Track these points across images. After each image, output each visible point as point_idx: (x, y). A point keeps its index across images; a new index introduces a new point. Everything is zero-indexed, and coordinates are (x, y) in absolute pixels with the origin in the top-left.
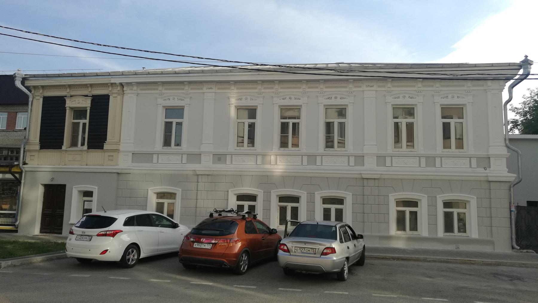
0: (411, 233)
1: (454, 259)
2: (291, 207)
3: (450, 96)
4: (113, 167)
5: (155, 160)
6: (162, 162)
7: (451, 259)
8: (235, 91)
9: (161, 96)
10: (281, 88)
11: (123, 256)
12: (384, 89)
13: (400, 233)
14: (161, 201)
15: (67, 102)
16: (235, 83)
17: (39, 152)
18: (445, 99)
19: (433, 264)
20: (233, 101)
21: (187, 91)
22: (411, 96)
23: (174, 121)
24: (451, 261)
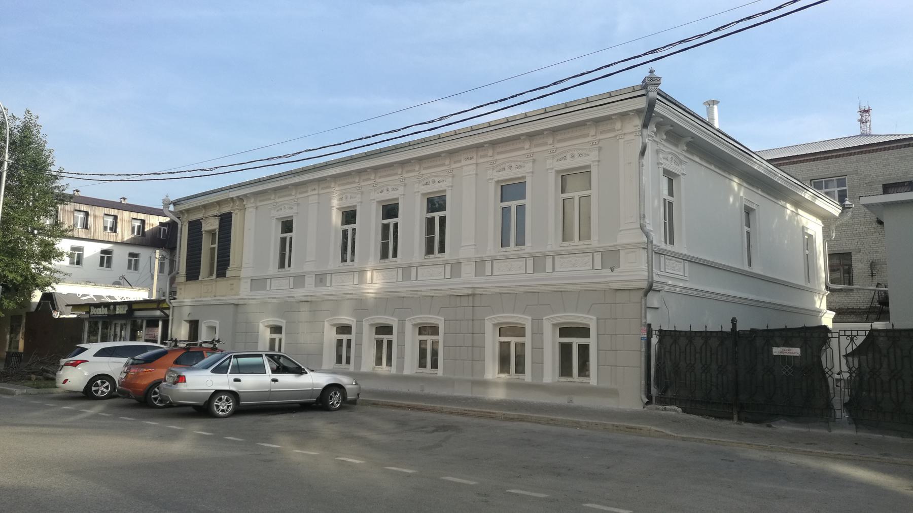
0: (517, 377)
1: (472, 411)
2: (579, 345)
3: (568, 155)
4: (224, 298)
5: (549, 268)
6: (561, 270)
7: (469, 411)
8: (337, 189)
9: (552, 154)
10: (558, 141)
11: (86, 387)
12: (587, 140)
13: (504, 376)
14: (504, 339)
15: (203, 225)
16: (554, 131)
17: (216, 281)
18: (563, 162)
19: (409, 412)
20: (335, 202)
21: (595, 137)
22: (519, 164)
23: (513, 204)
24: (469, 412)
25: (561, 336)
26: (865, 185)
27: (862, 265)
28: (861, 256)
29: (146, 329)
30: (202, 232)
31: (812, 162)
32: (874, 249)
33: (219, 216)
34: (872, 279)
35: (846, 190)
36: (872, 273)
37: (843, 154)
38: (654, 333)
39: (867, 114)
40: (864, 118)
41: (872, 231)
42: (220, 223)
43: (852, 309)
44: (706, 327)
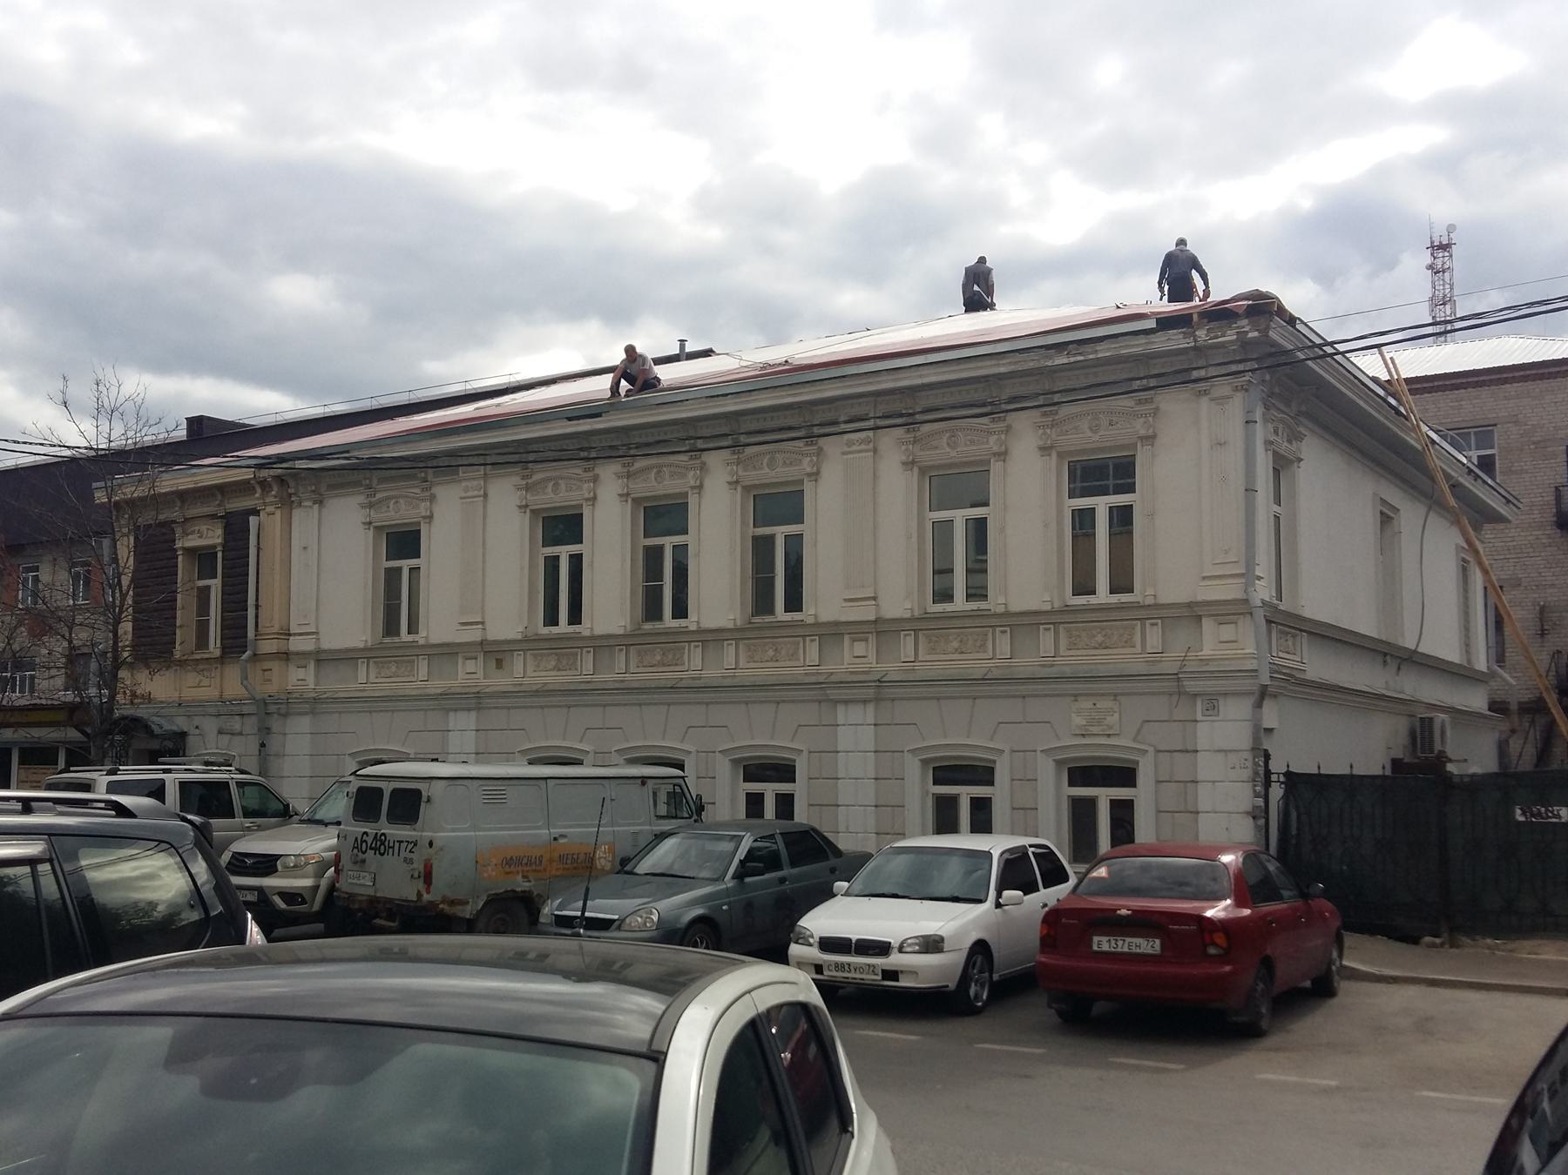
17: (222, 663)
25: (1072, 784)
26: (1532, 447)
27: (1523, 612)
28: (1522, 594)
29: (19, 769)
30: (176, 550)
31: (1426, 395)
32: (1549, 578)
33: (221, 517)
34: (1543, 642)
35: (1494, 455)
36: (1543, 630)
37: (1491, 380)
38: (1274, 777)
39: (1447, 254)
40: (1439, 262)
41: (1544, 541)
42: (225, 533)
43: (1501, 702)
44: (1351, 767)
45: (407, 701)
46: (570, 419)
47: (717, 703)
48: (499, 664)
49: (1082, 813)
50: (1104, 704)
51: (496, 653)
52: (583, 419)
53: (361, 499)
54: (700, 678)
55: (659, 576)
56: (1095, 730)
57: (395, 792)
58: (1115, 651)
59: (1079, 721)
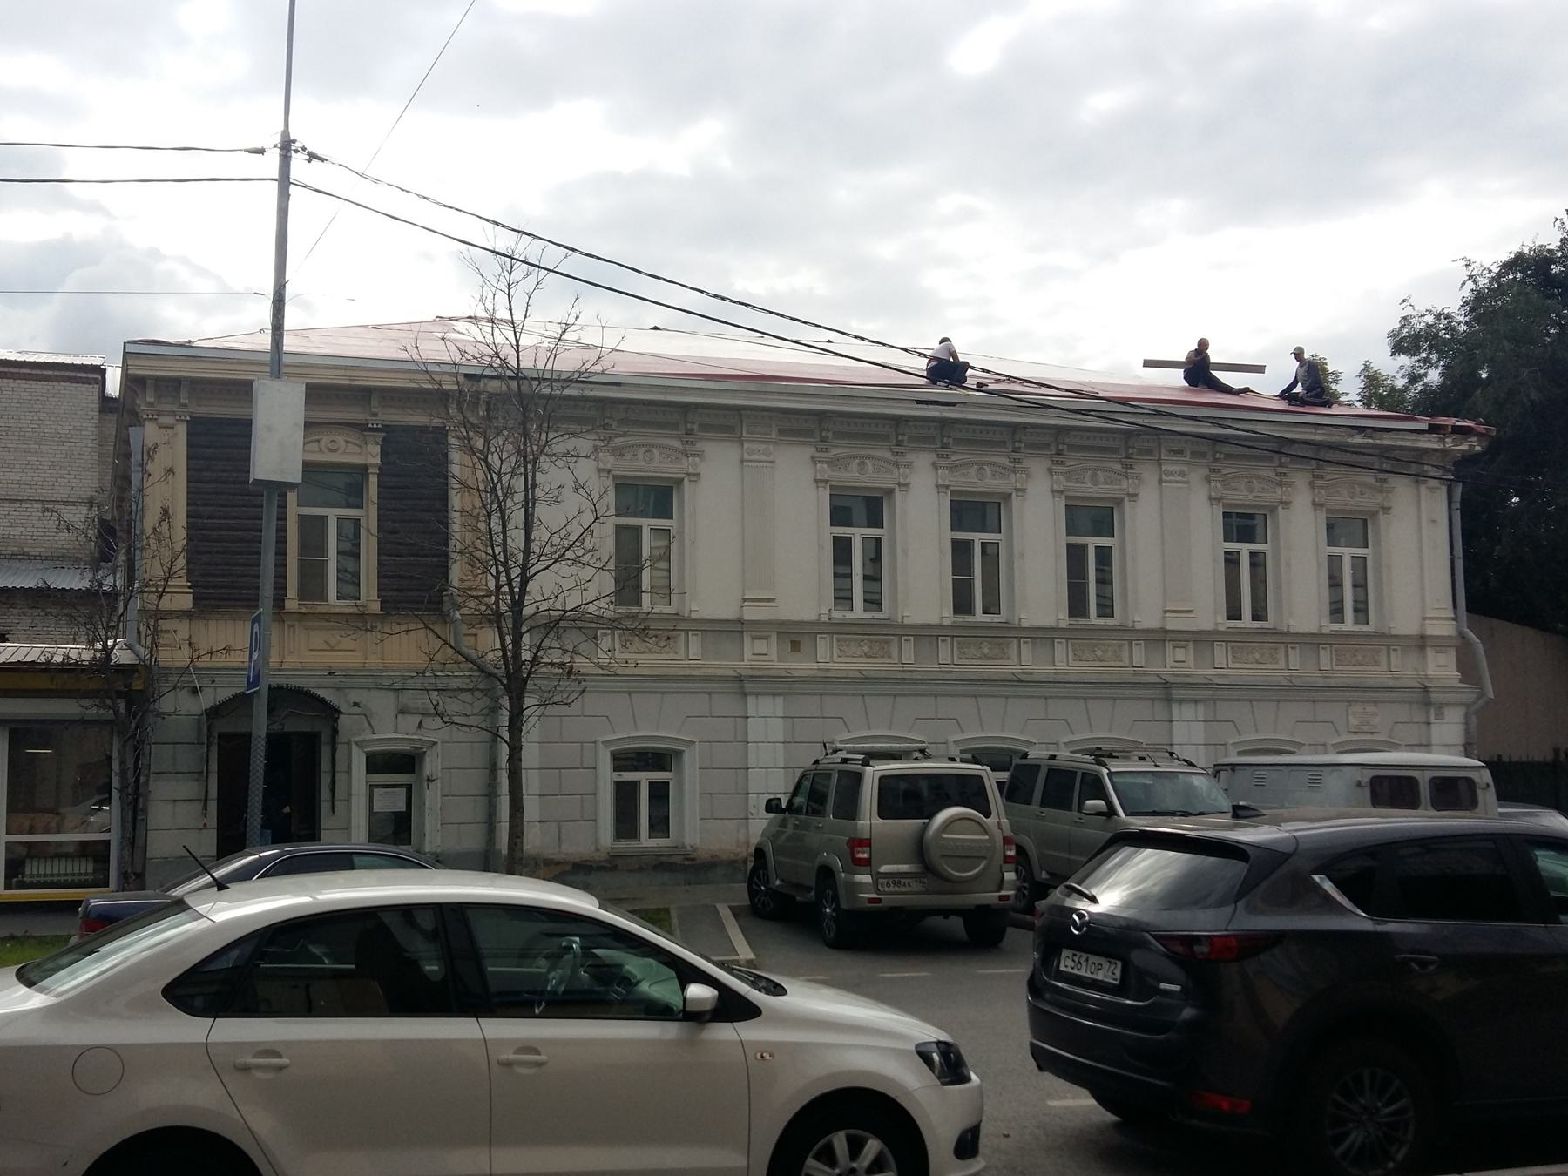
45: (688, 681)
46: (919, 402)
47: (905, 695)
48: (795, 646)
49: (625, 795)
50: (1371, 709)
51: (794, 635)
52: (932, 404)
53: (810, 451)
54: (1031, 673)
55: (969, 570)
56: (1365, 728)
57: (1433, 780)
58: (1368, 668)
59: (1353, 721)
